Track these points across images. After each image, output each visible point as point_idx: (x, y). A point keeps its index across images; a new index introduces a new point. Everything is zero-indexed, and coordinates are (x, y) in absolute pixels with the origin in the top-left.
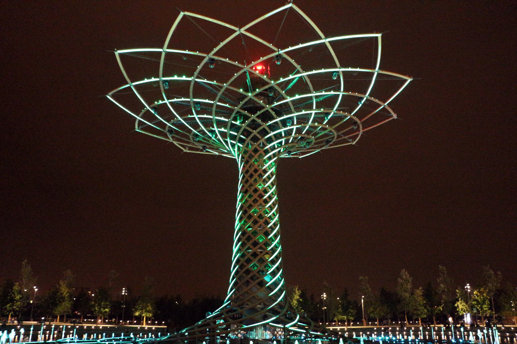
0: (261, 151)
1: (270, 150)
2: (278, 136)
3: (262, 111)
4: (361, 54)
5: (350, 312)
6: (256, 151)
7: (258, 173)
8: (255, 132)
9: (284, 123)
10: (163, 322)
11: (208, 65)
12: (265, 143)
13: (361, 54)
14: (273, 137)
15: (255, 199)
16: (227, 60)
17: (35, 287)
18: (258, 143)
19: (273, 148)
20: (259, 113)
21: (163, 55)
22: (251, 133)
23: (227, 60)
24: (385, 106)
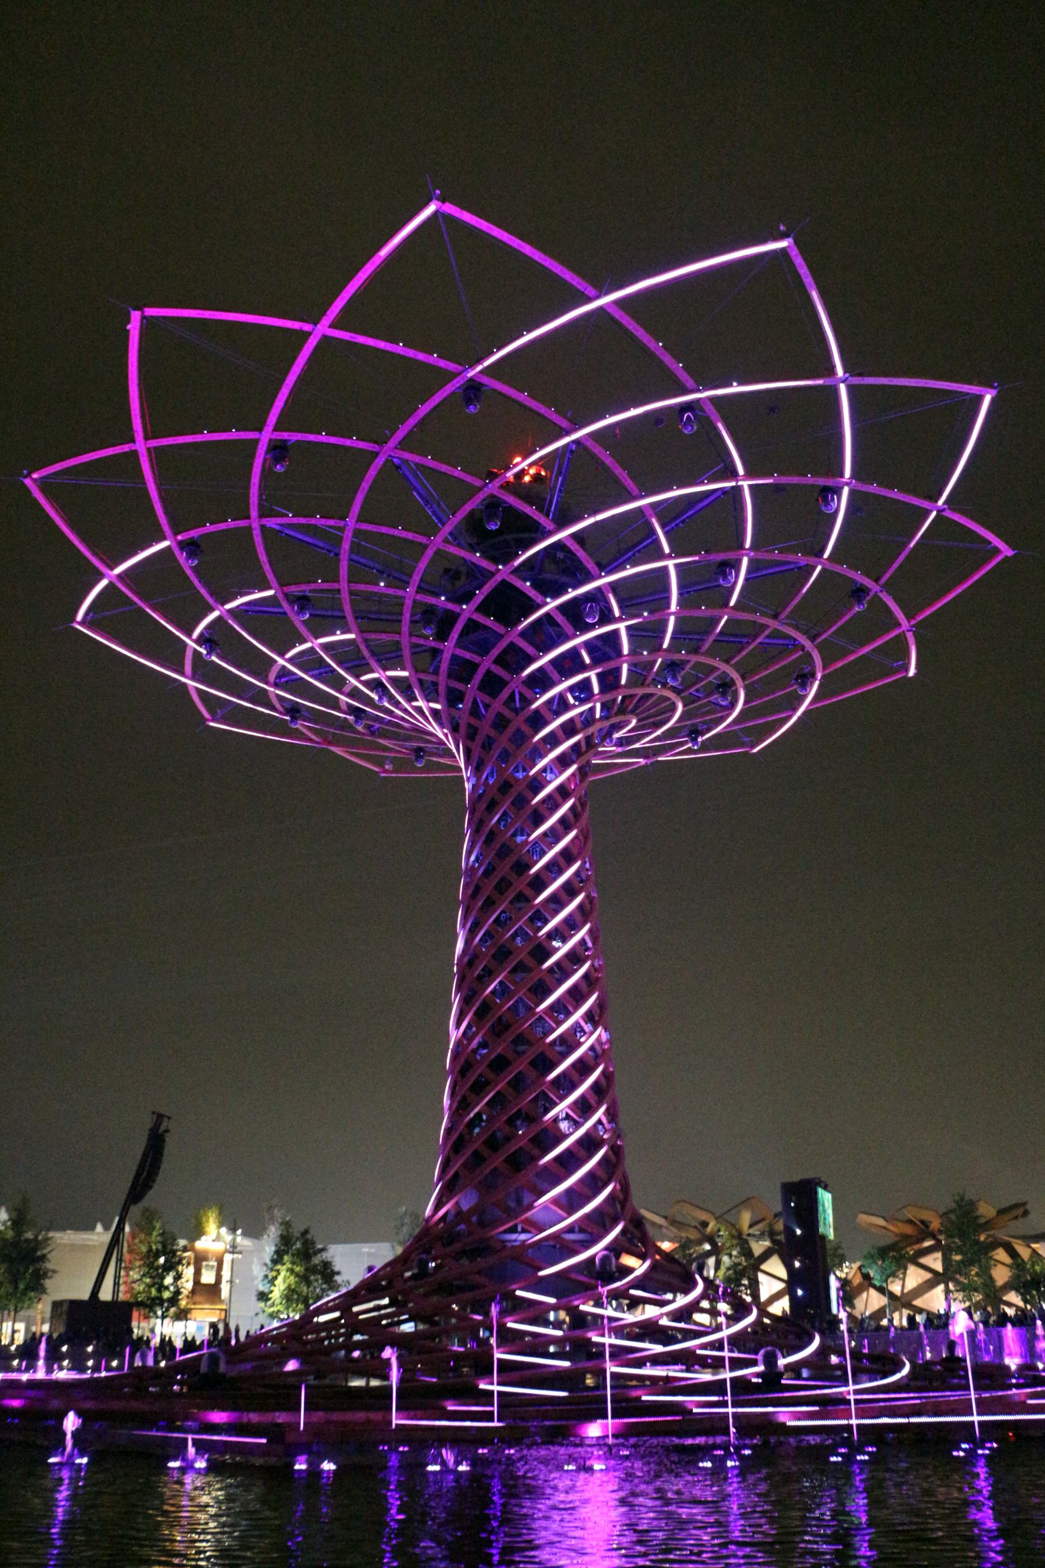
0: (518, 722)
1: (547, 715)
2: (569, 664)
3: (488, 588)
4: (749, 322)
5: (1030, 1294)
6: (500, 723)
7: (513, 793)
8: (487, 663)
9: (575, 615)
10: (90, 1349)
11: (270, 469)
12: (528, 693)
13: (749, 322)
14: (555, 676)
15: (503, 879)
16: (323, 437)
17: (507, 1452)
18: (505, 695)
19: (560, 705)
20: (480, 595)
21: (460, 652)
22: (474, 667)
23: (323, 437)
24: (940, 511)
